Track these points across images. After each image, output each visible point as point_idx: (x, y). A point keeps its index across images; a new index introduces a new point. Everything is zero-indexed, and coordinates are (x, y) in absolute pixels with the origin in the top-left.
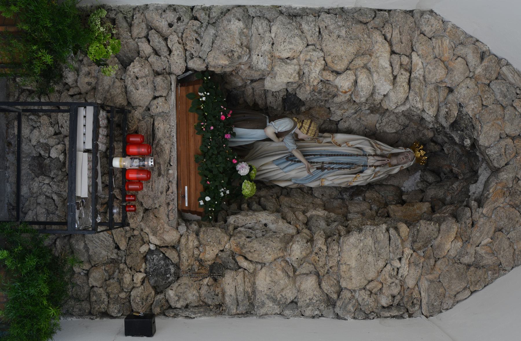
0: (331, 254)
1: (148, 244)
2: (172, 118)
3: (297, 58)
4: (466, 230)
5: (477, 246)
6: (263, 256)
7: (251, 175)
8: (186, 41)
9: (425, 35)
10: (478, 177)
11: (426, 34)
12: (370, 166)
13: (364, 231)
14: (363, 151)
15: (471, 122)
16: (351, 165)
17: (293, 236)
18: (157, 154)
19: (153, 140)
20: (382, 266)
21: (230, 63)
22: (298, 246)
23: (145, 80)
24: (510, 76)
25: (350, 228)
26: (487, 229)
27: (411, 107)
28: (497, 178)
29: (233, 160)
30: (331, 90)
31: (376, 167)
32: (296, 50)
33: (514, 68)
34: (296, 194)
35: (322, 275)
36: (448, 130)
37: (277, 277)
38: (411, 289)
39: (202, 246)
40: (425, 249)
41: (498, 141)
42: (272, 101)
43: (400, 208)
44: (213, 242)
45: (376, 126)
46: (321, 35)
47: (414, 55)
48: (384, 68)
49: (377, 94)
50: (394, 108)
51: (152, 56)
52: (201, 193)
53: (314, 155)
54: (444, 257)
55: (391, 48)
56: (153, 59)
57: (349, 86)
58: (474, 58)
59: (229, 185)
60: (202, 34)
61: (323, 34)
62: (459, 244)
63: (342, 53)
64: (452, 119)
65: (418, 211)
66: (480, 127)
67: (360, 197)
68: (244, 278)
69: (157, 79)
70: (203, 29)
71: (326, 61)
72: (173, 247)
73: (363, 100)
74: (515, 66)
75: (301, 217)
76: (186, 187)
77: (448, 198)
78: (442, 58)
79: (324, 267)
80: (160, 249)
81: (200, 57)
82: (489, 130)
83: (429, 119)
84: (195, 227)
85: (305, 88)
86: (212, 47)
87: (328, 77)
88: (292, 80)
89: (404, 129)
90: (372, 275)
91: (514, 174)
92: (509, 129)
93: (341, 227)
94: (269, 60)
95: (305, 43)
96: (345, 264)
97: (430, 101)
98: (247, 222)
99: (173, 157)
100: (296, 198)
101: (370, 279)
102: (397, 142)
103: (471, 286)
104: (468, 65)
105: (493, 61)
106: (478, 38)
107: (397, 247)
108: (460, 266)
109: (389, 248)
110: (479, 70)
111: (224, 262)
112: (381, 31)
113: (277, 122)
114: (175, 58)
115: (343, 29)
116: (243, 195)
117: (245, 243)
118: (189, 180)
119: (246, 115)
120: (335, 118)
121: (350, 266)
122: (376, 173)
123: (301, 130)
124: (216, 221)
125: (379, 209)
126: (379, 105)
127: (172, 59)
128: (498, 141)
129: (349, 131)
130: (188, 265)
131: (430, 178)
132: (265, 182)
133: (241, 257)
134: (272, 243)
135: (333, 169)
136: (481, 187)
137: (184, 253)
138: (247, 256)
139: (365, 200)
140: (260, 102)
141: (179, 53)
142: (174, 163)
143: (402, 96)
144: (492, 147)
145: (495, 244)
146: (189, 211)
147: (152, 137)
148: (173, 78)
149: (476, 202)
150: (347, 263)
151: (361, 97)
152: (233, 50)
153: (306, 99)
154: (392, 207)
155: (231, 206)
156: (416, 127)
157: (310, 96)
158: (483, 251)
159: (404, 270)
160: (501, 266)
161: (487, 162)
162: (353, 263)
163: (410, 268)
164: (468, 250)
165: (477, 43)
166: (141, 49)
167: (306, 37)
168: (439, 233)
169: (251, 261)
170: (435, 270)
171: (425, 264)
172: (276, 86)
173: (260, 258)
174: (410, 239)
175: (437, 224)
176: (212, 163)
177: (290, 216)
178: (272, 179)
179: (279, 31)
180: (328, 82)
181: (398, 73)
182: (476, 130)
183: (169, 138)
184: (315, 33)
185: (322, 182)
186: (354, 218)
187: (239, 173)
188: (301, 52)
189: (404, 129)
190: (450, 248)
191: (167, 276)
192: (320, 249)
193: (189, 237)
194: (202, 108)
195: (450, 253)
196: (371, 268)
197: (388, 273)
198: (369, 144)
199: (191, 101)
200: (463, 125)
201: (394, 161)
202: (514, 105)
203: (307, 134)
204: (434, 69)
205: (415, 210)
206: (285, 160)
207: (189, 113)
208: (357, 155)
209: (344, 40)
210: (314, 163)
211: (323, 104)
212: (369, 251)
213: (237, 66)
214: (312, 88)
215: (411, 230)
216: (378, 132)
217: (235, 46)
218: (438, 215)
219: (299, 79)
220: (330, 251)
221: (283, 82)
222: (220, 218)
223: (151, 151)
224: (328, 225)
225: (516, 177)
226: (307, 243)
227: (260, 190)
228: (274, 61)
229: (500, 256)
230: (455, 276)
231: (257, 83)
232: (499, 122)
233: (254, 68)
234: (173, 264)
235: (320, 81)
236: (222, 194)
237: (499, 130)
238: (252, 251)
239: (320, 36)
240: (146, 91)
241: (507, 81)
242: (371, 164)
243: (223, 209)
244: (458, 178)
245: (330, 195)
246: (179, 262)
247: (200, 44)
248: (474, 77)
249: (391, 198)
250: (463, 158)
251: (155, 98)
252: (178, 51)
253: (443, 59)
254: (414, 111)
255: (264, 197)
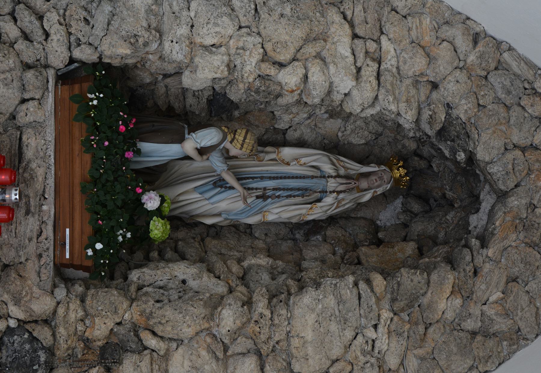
0: (276, 321)
1: (7, 319)
2: (48, 130)
3: (225, 45)
4: (466, 281)
5: (483, 304)
6: (179, 328)
7: (163, 209)
8: (70, 20)
9: (397, 13)
10: (480, 204)
11: (398, 10)
12: (331, 192)
13: (322, 286)
14: (321, 171)
15: (464, 128)
16: (304, 191)
17: (222, 297)
18: (25, 182)
19: (20, 162)
20: (351, 337)
21: (132, 53)
22: (229, 311)
23: (9, 76)
24: (514, 65)
25: (304, 282)
26: (495, 278)
27: (382, 109)
28: (505, 205)
29: (137, 189)
30: (273, 88)
31: (339, 193)
32: (225, 35)
33: (519, 54)
34: (228, 235)
35: (265, 354)
36: (434, 140)
37: (200, 361)
38: (394, 371)
39: (89, 317)
40: (410, 311)
41: (503, 154)
42: (193, 103)
43: (375, 250)
44: (107, 311)
45: (337, 136)
46: (258, 13)
47: (384, 39)
48: (344, 58)
49: (335, 93)
50: (359, 111)
51: (20, 41)
52: (89, 238)
53: (253, 178)
54: (437, 322)
55: (352, 30)
56: (21, 45)
57: (297, 83)
58: (464, 42)
59: (130, 225)
60: (93, 11)
61: (261, 12)
62: (458, 302)
63: (287, 38)
64: (437, 125)
65: (400, 255)
66: (476, 136)
67: (318, 237)
68: (152, 365)
69: (27, 74)
70: (95, 5)
71: (265, 48)
72: (46, 322)
73: (317, 101)
74: (521, 51)
75: (235, 268)
76: (68, 230)
77: (441, 235)
78: (421, 43)
79: (268, 341)
80: (25, 325)
81: (90, 44)
82: (490, 139)
83: (407, 126)
84: (79, 289)
85: (238, 86)
86: (107, 30)
87: (268, 71)
88: (220, 75)
89: (377, 138)
90: (336, 352)
91: (528, 200)
92: (516, 137)
93: (290, 282)
94: (187, 48)
95: (236, 24)
96: (298, 336)
97: (407, 101)
98: (156, 278)
99: (48, 186)
100: (229, 241)
101: (335, 358)
102: (367, 157)
103: (479, 364)
104: (456, 52)
105: (491, 45)
106: (469, 15)
107: (370, 307)
108: (461, 334)
109: (360, 310)
110: (472, 58)
111: (122, 341)
112: (339, 8)
113: (199, 134)
114: (54, 44)
115: (287, 6)
116: (151, 238)
117: (154, 311)
118: (73, 219)
119: (155, 124)
120: (282, 125)
121: (305, 339)
122: (339, 202)
123: (233, 143)
124: (112, 278)
125: (345, 254)
126: (340, 108)
127: (50, 46)
128: (503, 154)
129: (301, 144)
130: (68, 349)
131: (416, 207)
132: (185, 218)
133: (147, 332)
134: (192, 308)
135: (279, 197)
136: (485, 218)
137: (62, 330)
138: (156, 330)
139: (325, 241)
140: (176, 105)
141: (59, 37)
142: (50, 194)
143: (369, 95)
144: (494, 162)
145: (508, 301)
146: (71, 265)
147: (17, 157)
148: (51, 73)
149: (477, 241)
150: (301, 335)
151: (314, 98)
152: (138, 34)
153: (241, 101)
154: (363, 249)
155: (135, 255)
156: (393, 135)
157: (245, 96)
158: (493, 312)
159: (382, 344)
160: (519, 333)
161: (489, 183)
162: (309, 335)
163: (391, 339)
164: (470, 310)
165: (467, 21)
166: (3, 31)
167: (237, 17)
168: (428, 286)
169: (162, 338)
170: (426, 342)
171: (411, 332)
172: (197, 84)
173: (175, 332)
174: (389, 296)
175: (425, 273)
176: (105, 194)
177: (219, 266)
178: (194, 213)
179: (200, 8)
180: (269, 78)
181: (363, 64)
182: (472, 139)
183: (44, 158)
184: (250, 11)
185: (264, 216)
186: (311, 267)
187: (145, 206)
188: (231, 37)
189: (377, 138)
190: (445, 308)
191: (35, 368)
192: (261, 315)
193: (71, 305)
194: (93, 115)
195: (446, 316)
196: (335, 341)
197: (359, 349)
198: (329, 162)
199: (76, 106)
200: (454, 133)
201: (364, 184)
202: (522, 104)
203: (241, 149)
204: (411, 58)
205: (396, 253)
206: (212, 186)
207: (74, 122)
208: (313, 177)
209: (289, 20)
210: (252, 189)
211: (262, 106)
212: (332, 315)
213: (144, 56)
214: (247, 85)
215: (388, 283)
216: (342, 143)
217: (139, 29)
218: (427, 260)
219: (229, 74)
220: (275, 317)
221: (206, 78)
222: (117, 274)
223: (15, 178)
224: (273, 279)
225: (531, 203)
226: (242, 307)
227: (178, 229)
228: (193, 50)
229: (517, 318)
230: (455, 350)
231: (171, 78)
232: (503, 128)
233: (166, 60)
234: (43, 348)
235: (257, 76)
236: (120, 239)
237: (503, 139)
238: (163, 321)
239: (257, 15)
240: (10, 91)
241: (511, 72)
242: (331, 190)
243: (121, 260)
244: (453, 206)
245: (276, 235)
246: (54, 344)
247: (91, 26)
248: (465, 67)
249: (361, 237)
250: (458, 178)
251: (24, 101)
252: (58, 35)
253: (422, 43)
254: (387, 116)
255: (183, 240)
